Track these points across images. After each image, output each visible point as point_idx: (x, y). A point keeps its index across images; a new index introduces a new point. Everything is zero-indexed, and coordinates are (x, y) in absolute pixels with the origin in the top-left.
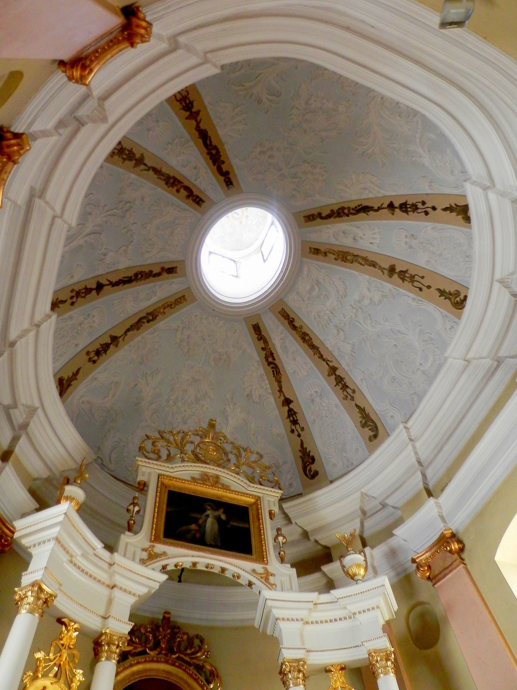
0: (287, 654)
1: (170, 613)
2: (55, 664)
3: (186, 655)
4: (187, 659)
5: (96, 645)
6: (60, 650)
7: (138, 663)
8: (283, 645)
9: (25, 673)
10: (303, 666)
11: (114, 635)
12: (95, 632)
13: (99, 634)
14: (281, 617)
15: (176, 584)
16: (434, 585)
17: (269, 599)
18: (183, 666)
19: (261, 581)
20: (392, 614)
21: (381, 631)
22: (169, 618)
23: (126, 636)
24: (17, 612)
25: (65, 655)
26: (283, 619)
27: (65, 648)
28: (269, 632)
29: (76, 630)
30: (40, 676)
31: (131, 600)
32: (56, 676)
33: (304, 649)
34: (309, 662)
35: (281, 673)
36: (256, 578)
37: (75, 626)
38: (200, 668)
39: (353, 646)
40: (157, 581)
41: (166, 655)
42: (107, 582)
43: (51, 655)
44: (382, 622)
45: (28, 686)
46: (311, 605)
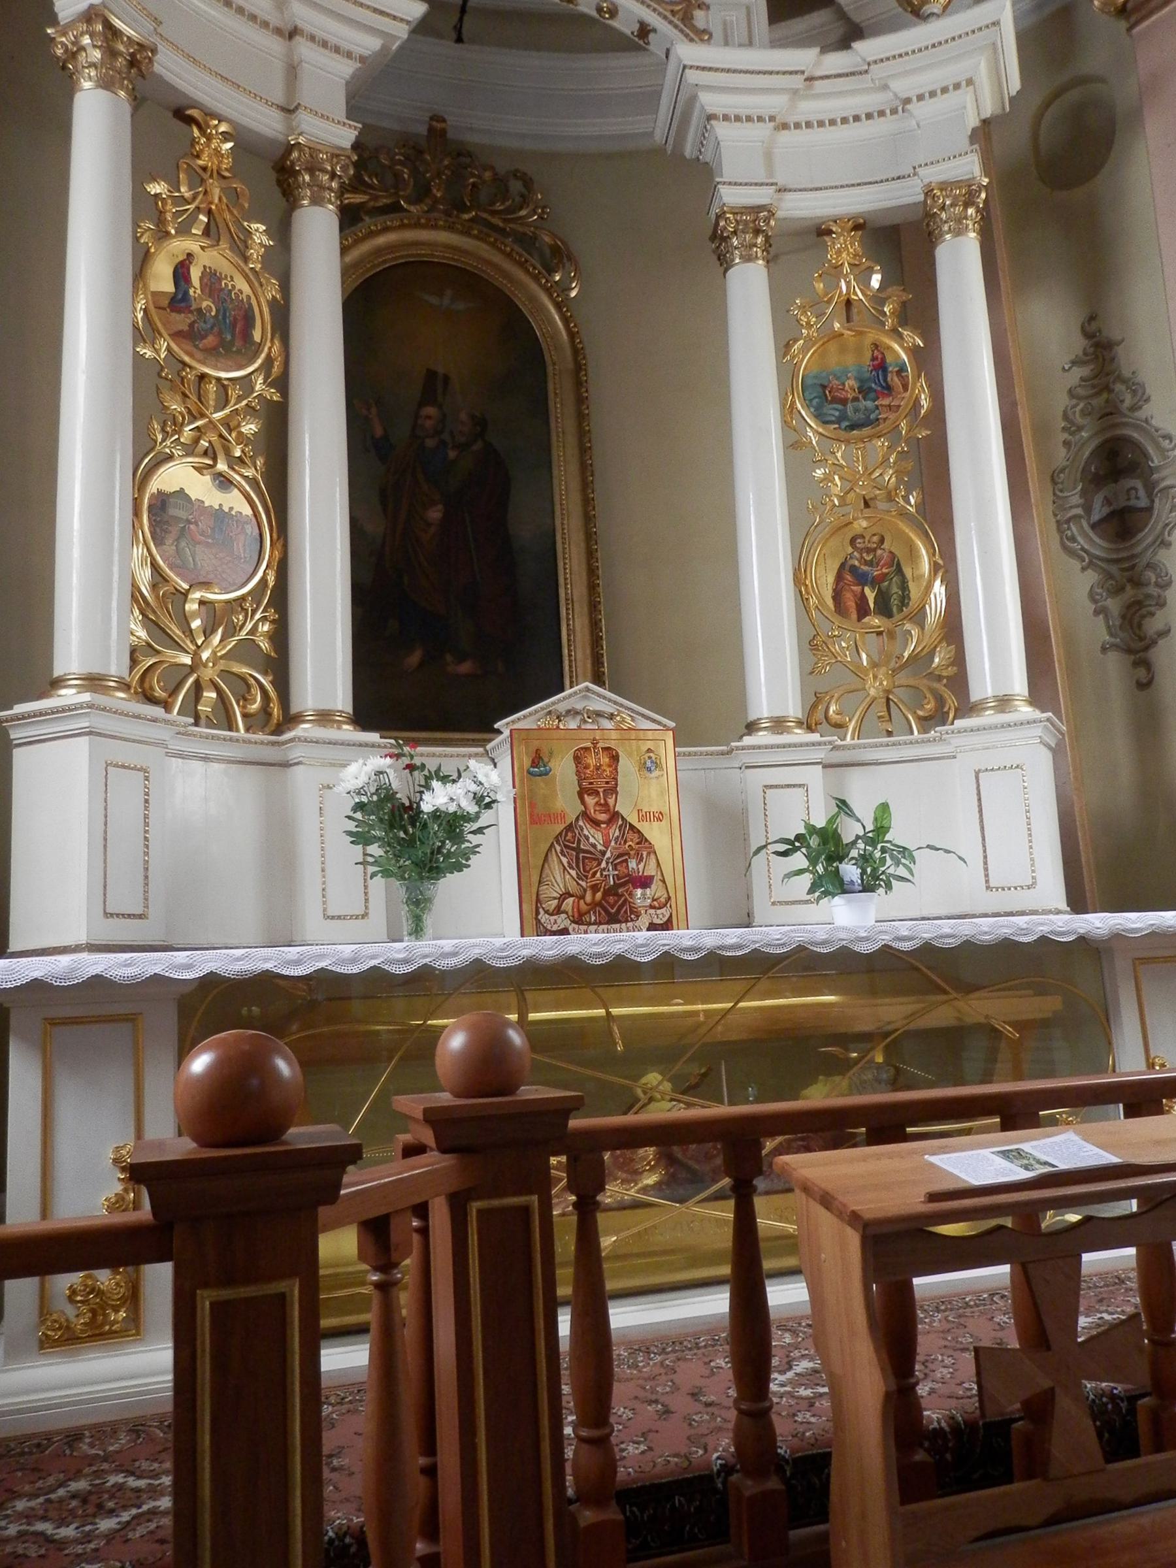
0: (730, 196)
1: (444, 121)
2: (198, 208)
3: (494, 213)
4: (496, 221)
5: (280, 174)
6: (203, 181)
7: (386, 230)
8: (722, 176)
9: (136, 225)
10: (767, 220)
11: (321, 152)
12: (273, 142)
13: (282, 151)
14: (720, 111)
15: (448, 48)
16: (1129, 29)
17: (691, 67)
18: (490, 236)
19: (671, 22)
20: (1003, 103)
21: (966, 141)
22: (443, 132)
23: (349, 152)
24: (69, 88)
25: (216, 193)
26: (726, 118)
27: (211, 176)
28: (689, 151)
29: (226, 137)
30: (173, 232)
31: (347, 69)
32: (207, 232)
33: (772, 184)
34: (780, 214)
35: (714, 236)
36: (660, 14)
37: (222, 129)
38: (528, 241)
39: (890, 176)
40: (402, 20)
41: (447, 213)
42: (274, 21)
43: (182, 190)
44: (973, 121)
45: (152, 250)
46: (797, 82)
